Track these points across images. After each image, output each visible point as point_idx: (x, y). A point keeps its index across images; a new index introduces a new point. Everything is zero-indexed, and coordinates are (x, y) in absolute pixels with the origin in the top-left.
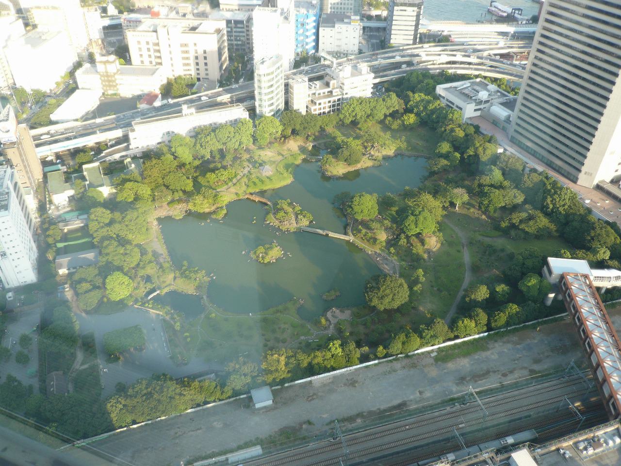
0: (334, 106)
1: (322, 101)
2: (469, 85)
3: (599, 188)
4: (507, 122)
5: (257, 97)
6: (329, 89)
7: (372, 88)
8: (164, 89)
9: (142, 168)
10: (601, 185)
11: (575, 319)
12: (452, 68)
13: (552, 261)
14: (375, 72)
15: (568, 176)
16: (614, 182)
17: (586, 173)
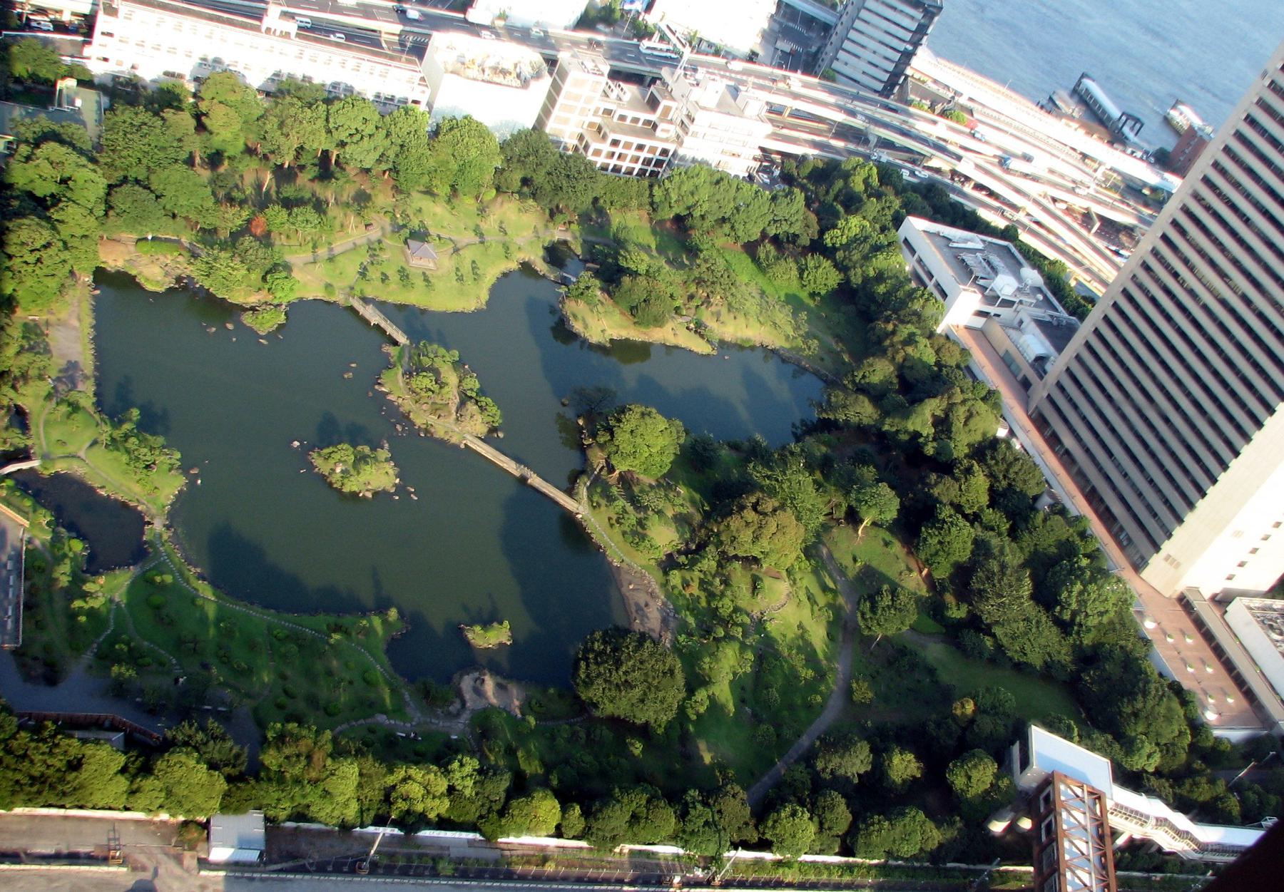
2: (980, 246)
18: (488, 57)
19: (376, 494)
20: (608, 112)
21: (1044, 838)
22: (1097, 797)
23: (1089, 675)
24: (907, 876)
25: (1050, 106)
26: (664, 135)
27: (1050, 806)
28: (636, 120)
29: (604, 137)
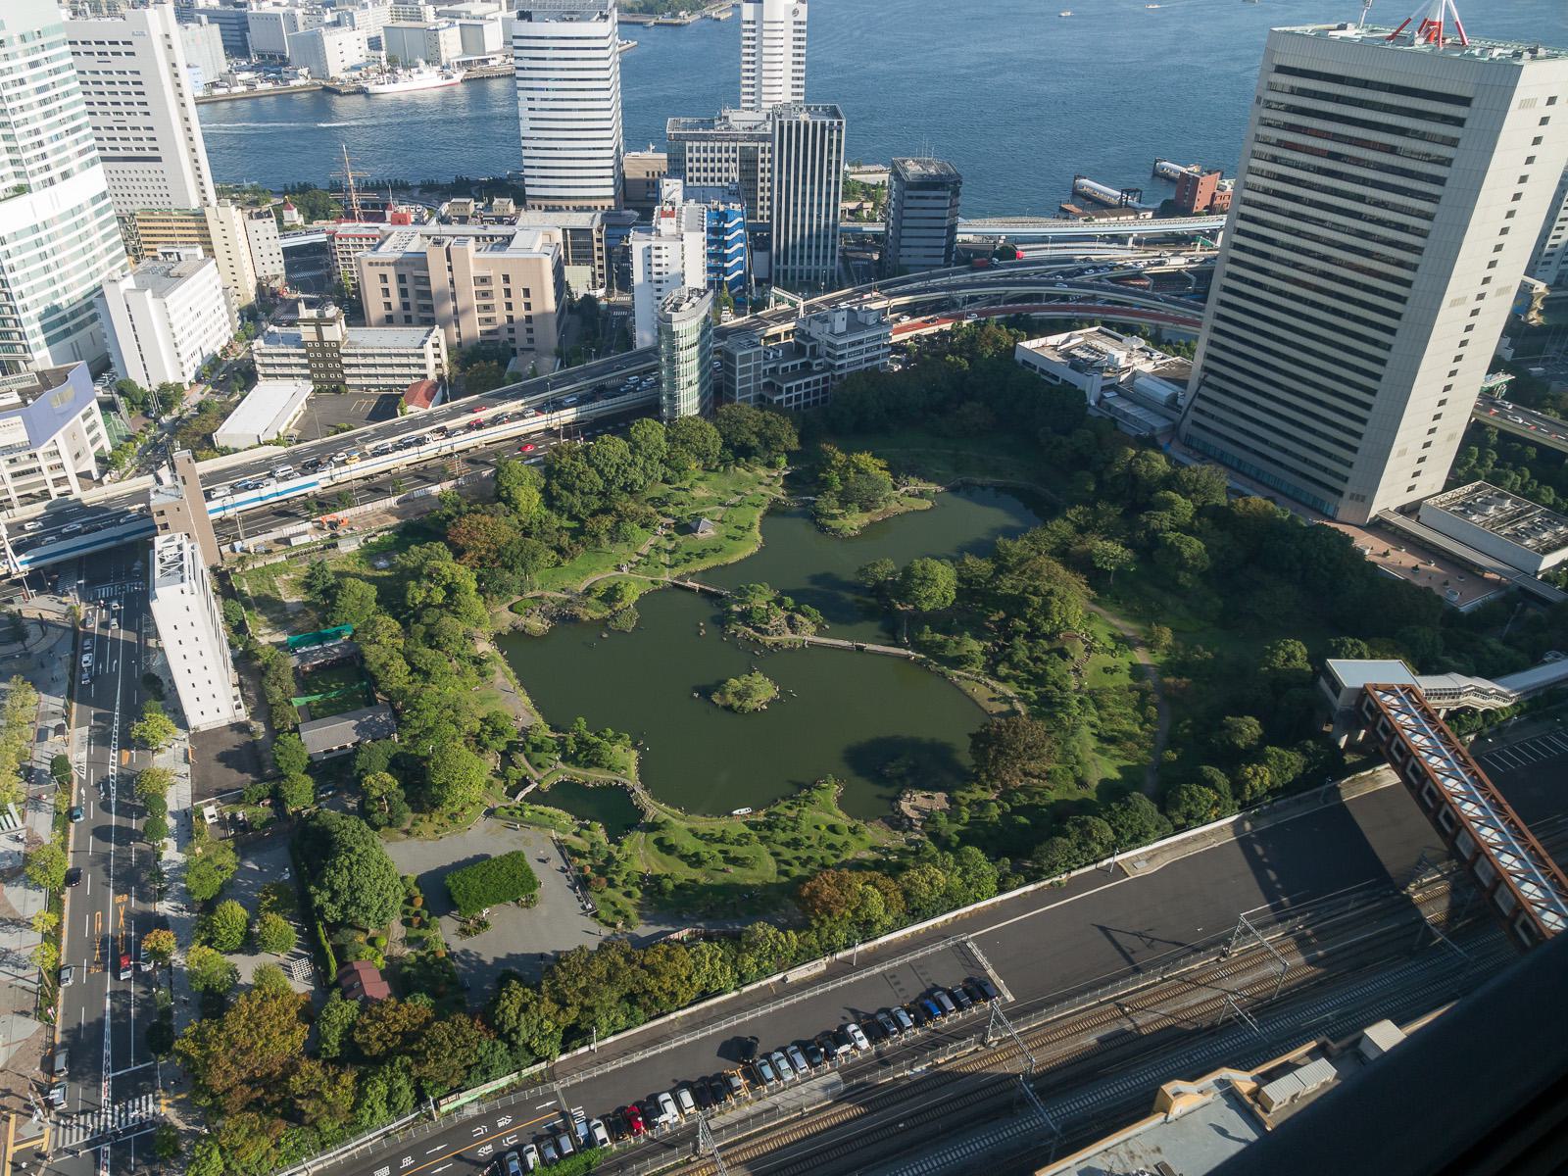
7: (496, 959)
8: (457, 362)
11: (1517, 936)
17: (1352, 497)
18: (167, 36)
21: (1384, 738)
22: (1410, 690)
23: (774, 661)
24: (770, 401)
25: (1066, 214)
26: (819, 368)
27: (1377, 711)
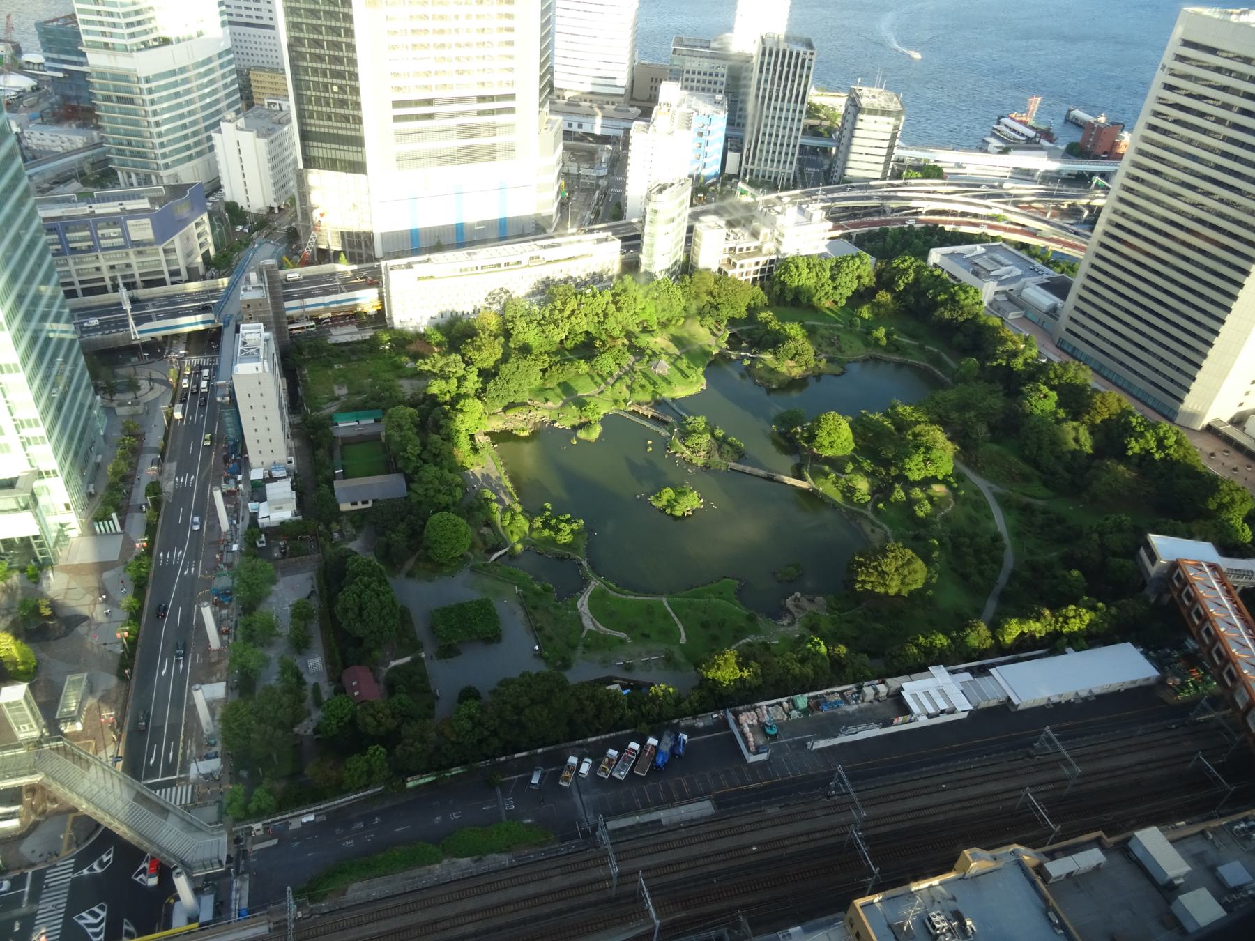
0: (763, 271)
1: (745, 262)
2: (983, 250)
3: (1209, 429)
4: (1052, 316)
5: (645, 249)
6: (757, 243)
9: (377, 750)
10: (1216, 426)
12: (950, 223)
13: (1154, 539)
14: (834, 220)
15: (81, 64)
16: (1239, 421)
19: (693, 511)
20: (732, 249)
28: (748, 249)
29: (735, 265)
